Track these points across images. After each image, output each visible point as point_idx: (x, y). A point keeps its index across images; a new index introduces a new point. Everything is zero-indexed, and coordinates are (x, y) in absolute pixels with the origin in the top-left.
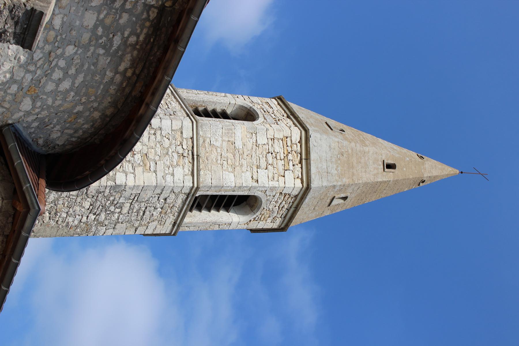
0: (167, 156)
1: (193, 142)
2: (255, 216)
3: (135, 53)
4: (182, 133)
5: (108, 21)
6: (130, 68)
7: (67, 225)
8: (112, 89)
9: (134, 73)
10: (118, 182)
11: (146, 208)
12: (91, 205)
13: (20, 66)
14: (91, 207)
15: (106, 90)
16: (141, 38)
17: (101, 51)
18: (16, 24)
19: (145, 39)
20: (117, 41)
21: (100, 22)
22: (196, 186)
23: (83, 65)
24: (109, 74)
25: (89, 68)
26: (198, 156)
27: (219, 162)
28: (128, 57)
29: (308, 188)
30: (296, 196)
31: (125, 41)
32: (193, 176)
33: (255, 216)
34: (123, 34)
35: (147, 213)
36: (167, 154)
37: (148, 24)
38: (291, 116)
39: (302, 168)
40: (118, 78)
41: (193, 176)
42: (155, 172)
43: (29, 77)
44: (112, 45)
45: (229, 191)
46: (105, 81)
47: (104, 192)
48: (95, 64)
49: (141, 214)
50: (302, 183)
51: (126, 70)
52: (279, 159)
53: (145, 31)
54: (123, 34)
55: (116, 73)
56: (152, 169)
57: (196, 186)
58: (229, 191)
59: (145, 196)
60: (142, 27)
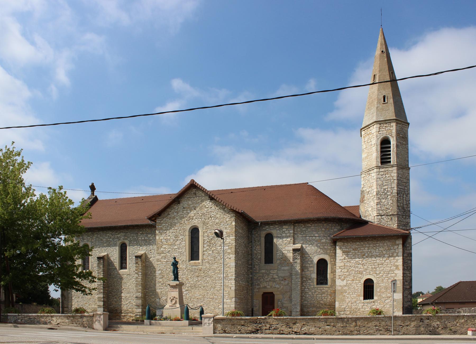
0: (370, 180)
1: (366, 172)
2: (390, 136)
3: (306, 224)
4: (364, 177)
5: (300, 233)
6: (310, 223)
7: (392, 203)
8: (316, 225)
9: (311, 222)
10: (375, 194)
11: (385, 180)
12: (384, 199)
13: (313, 245)
14: (385, 199)
15: (317, 226)
16: (302, 224)
17: (307, 231)
18: (296, 252)
19: (302, 224)
20: (304, 229)
21: (300, 234)
22: (376, 168)
23: (311, 234)
24: (312, 227)
25: (311, 232)
26: (369, 170)
27: (370, 161)
28: (307, 225)
29: (375, 122)
30: (380, 124)
31: (303, 228)
32: (374, 169)
33: (390, 136)
34: (302, 229)
35: (388, 179)
36: (369, 180)
37: (299, 225)
38: (369, 127)
39: (371, 127)
40: (313, 225)
41: (374, 169)
42: (373, 183)
43: (315, 243)
44: (305, 230)
45: (378, 153)
46: (314, 227)
47: (379, 197)
48: (310, 231)
49: (388, 181)
50: (374, 125)
51: (311, 224)
52: (177, 312)
53: (301, 224)
54: (302, 229)
55: (312, 226)
56: (372, 184)
57: (376, 168)
58: (378, 153)
59: (236, 270)
60: (300, 225)
